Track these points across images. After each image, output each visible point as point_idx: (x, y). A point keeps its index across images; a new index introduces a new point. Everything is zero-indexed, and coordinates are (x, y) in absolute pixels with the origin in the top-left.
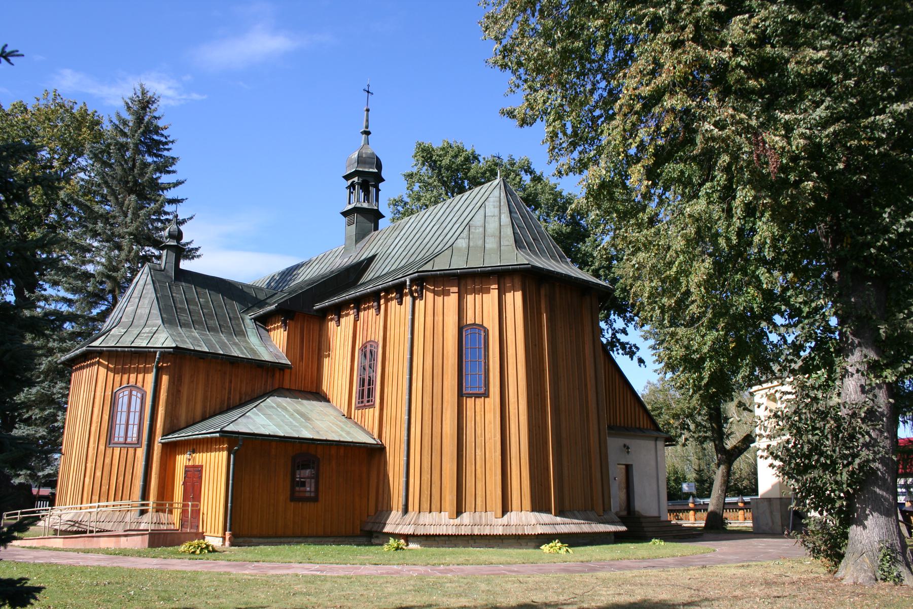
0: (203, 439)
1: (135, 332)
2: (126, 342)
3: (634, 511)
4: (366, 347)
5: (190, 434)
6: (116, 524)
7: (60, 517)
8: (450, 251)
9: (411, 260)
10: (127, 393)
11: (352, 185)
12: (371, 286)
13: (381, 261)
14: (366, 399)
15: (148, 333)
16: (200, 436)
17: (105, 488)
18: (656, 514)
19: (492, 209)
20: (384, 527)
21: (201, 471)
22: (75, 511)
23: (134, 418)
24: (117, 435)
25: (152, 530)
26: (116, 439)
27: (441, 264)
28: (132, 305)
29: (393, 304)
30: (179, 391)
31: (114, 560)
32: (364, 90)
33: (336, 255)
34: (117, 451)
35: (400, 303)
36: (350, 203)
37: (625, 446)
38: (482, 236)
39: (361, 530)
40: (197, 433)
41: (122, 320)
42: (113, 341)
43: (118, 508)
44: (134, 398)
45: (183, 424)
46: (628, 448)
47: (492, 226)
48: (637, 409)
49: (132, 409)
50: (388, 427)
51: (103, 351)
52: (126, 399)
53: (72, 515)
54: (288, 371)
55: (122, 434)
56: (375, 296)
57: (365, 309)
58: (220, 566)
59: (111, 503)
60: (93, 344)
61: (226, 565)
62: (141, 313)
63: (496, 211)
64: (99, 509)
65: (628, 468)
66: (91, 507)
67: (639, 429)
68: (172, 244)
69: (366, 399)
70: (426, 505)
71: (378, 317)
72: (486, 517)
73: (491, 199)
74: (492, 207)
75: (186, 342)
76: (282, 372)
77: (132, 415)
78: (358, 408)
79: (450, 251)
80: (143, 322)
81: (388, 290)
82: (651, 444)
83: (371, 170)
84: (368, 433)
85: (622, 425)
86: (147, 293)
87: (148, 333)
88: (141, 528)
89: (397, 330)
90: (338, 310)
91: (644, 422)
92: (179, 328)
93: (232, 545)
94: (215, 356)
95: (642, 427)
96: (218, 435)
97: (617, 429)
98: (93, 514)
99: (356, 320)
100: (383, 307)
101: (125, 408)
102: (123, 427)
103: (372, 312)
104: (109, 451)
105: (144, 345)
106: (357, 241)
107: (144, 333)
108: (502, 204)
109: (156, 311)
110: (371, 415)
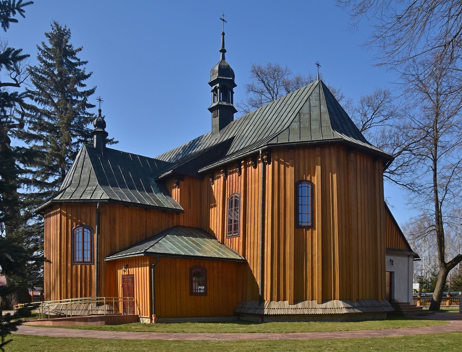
0: (133, 257)
1: (82, 190)
2: (76, 197)
3: (394, 300)
4: (232, 198)
5: (124, 255)
6: (83, 311)
7: (49, 307)
8: (287, 131)
9: (260, 139)
10: (81, 230)
11: (215, 90)
12: (235, 156)
13: (238, 141)
14: (233, 231)
15: (90, 190)
16: (131, 256)
17: (74, 290)
18: (405, 301)
19: (315, 102)
20: (264, 312)
21: (133, 278)
22: (57, 304)
23: (87, 246)
24: (77, 257)
25: (106, 314)
26: (77, 260)
27: (282, 140)
28: (78, 173)
29: (250, 169)
30: (114, 228)
31: (86, 333)
32: (221, 19)
33: (206, 138)
34: (79, 266)
35: (255, 167)
36: (214, 102)
37: (390, 260)
38: (308, 120)
39: (233, 312)
40: (129, 254)
41: (72, 182)
42: (68, 196)
43: (83, 302)
44: (85, 233)
45: (118, 249)
46: (393, 262)
47: (315, 113)
48: (399, 238)
49: (85, 240)
50: (249, 249)
51: (62, 202)
52: (81, 234)
53: (56, 306)
54: (182, 215)
55: (81, 256)
56: (237, 164)
57: (230, 174)
58: (153, 335)
59: (79, 298)
60: (56, 198)
61: (157, 335)
62: (84, 178)
63: (318, 103)
64: (72, 302)
65: (391, 274)
66: (67, 301)
67: (399, 250)
68: (99, 130)
69: (233, 231)
70: (275, 296)
71: (239, 177)
72: (312, 304)
73: (313, 95)
74: (314, 100)
75: (115, 196)
76: (178, 215)
77: (85, 244)
78: (228, 237)
79: (287, 131)
80: (86, 183)
81: (246, 158)
82: (406, 259)
83: (230, 78)
84: (237, 254)
85: (390, 247)
86: (87, 164)
87: (90, 190)
88: (99, 313)
89: (253, 186)
90: (213, 174)
91: (402, 247)
92: (110, 187)
93: (156, 322)
94: (136, 204)
95: (401, 249)
96: (143, 254)
97: (391, 251)
98: (68, 305)
99: (225, 180)
100: (243, 170)
101: (81, 240)
102: (81, 252)
103: (235, 175)
104: (74, 267)
105: (89, 198)
106: (220, 129)
107: (87, 191)
108: (321, 98)
109: (94, 176)
110: (237, 241)
